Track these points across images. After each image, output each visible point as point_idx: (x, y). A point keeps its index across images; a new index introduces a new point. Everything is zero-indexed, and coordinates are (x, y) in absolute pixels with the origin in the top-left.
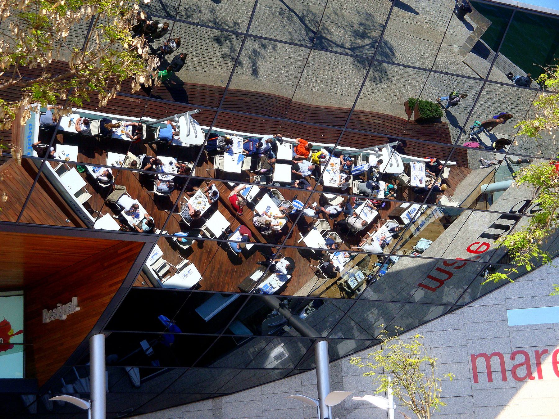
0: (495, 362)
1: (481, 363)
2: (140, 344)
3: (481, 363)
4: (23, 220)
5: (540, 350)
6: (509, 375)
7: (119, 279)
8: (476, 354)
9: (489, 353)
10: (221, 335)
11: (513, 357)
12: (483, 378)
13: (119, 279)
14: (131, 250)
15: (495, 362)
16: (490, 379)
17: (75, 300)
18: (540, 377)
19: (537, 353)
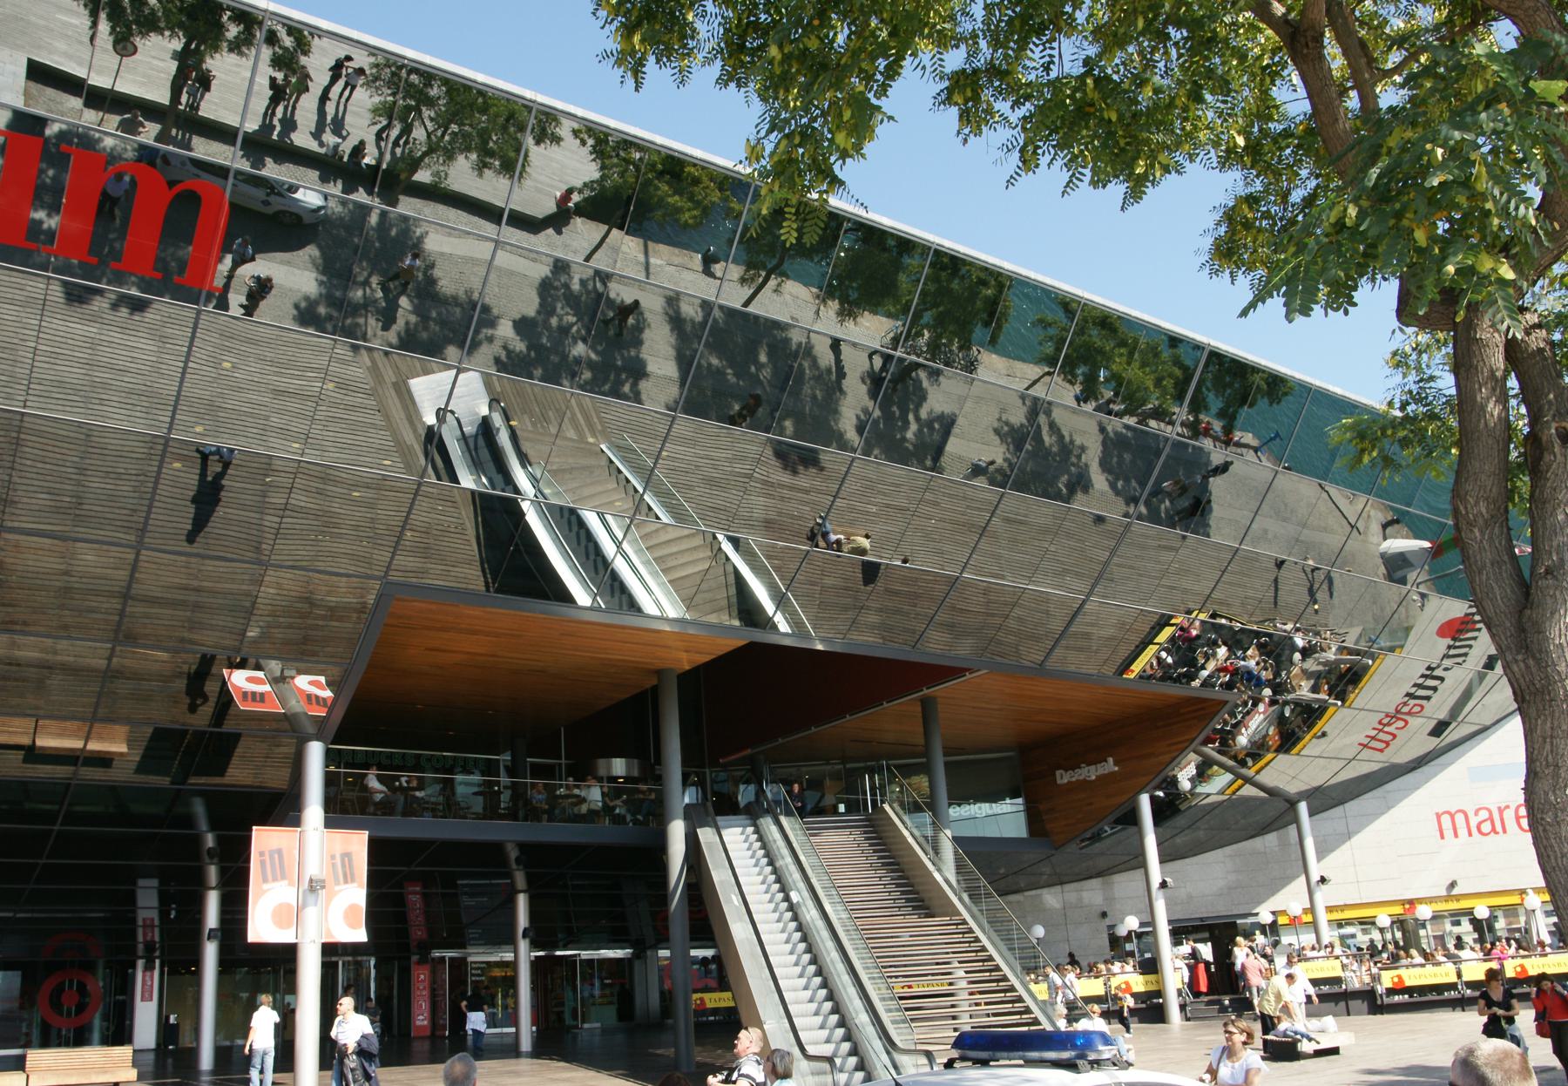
0: (1460, 818)
1: (1446, 820)
2: (246, 843)
3: (1446, 820)
4: (1052, 664)
5: (1503, 806)
6: (1474, 830)
7: (1186, 737)
8: (1440, 811)
9: (1453, 811)
10: (56, 828)
11: (1476, 813)
12: (1449, 833)
13: (1186, 737)
14: (1203, 709)
15: (1460, 818)
16: (1456, 835)
17: (1111, 760)
18: (1505, 831)
19: (1499, 808)
